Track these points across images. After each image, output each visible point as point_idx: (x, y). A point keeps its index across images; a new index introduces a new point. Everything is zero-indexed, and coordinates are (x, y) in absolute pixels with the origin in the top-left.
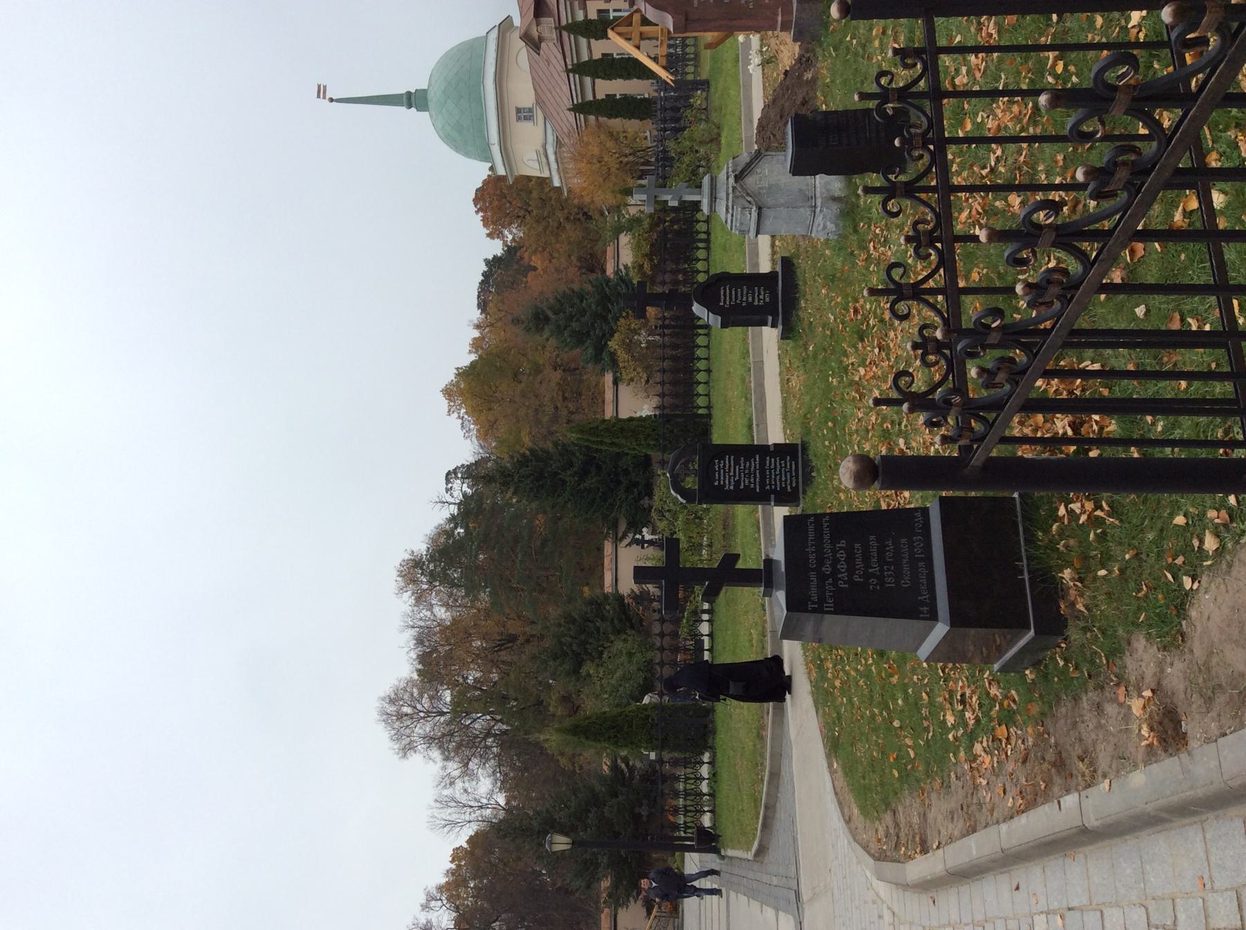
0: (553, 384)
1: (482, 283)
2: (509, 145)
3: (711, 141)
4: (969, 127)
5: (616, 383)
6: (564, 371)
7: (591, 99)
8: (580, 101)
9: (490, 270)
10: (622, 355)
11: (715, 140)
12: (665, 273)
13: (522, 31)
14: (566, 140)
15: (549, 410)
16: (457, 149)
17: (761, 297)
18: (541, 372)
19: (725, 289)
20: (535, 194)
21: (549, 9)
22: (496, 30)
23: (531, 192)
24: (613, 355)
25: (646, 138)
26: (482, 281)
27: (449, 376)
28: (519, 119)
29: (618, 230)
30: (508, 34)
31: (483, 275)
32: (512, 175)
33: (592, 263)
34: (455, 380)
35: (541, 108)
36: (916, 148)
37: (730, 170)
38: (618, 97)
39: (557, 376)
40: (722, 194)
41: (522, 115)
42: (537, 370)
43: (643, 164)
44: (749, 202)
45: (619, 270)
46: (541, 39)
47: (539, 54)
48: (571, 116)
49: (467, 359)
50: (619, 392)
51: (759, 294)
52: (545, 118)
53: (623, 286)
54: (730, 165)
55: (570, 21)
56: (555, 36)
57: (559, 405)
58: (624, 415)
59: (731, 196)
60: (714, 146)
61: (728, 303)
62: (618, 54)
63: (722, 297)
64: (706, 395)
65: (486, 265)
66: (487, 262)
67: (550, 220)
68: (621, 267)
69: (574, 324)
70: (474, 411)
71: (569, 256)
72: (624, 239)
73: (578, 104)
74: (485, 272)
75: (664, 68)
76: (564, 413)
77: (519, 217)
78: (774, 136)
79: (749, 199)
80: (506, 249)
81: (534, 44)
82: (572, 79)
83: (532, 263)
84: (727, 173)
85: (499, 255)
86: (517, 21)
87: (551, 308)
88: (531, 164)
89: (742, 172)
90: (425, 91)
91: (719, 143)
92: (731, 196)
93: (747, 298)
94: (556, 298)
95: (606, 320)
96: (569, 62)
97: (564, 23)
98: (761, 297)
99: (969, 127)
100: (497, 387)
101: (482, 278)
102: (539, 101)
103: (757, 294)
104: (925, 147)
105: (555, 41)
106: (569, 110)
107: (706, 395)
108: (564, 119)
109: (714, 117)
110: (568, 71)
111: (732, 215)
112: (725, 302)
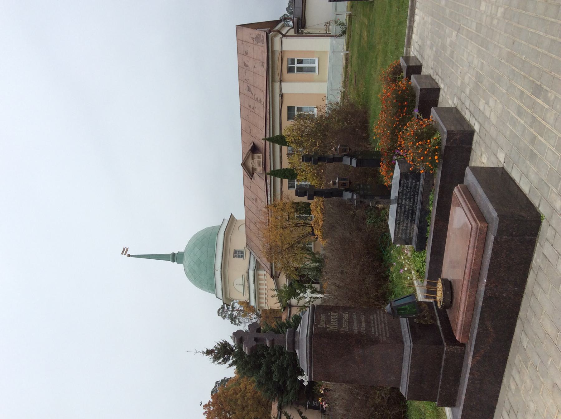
28: (235, 256)
41: (237, 255)
55: (271, 136)
82: (268, 181)
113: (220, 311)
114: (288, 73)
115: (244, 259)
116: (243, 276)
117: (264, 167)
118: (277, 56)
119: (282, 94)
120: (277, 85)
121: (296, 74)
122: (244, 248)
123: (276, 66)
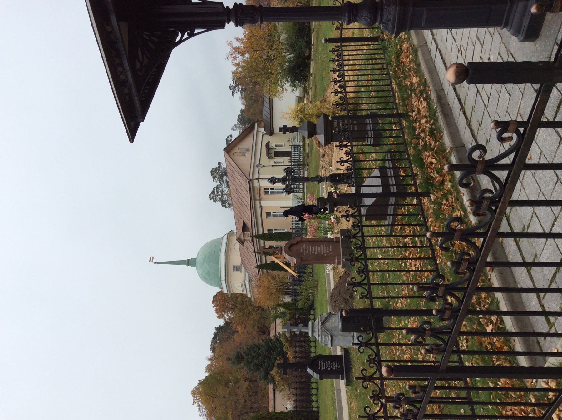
0: (244, 389)
1: (213, 338)
2: (229, 280)
3: (314, 287)
4: (403, 324)
5: (274, 390)
6: (250, 381)
7: (265, 263)
8: (260, 264)
9: (217, 332)
10: (277, 378)
11: (316, 286)
12: (296, 342)
13: (237, 237)
14: (254, 279)
15: (242, 401)
16: (207, 283)
17: (336, 366)
18: (238, 382)
19: (321, 362)
20: (239, 299)
21: (248, 229)
22: (226, 236)
23: (238, 298)
24: (273, 378)
25: (288, 278)
26: (214, 337)
27: (195, 384)
28: (234, 270)
29: (276, 317)
30: (231, 237)
31: (214, 334)
32: (230, 293)
33: (264, 330)
34: (197, 386)
35: (244, 266)
36: (372, 364)
37: (319, 320)
39: (246, 384)
40: (317, 330)
41: (236, 268)
42: (237, 381)
43: (287, 289)
44: (327, 333)
45: (276, 335)
46: (245, 240)
48: (256, 270)
49: (203, 375)
50: (276, 394)
51: (335, 365)
53: (278, 343)
54: (319, 318)
55: (257, 234)
57: (247, 400)
58: (278, 410)
59: (320, 331)
60: (315, 289)
61: (322, 368)
62: (276, 246)
63: (320, 366)
64: (316, 401)
65: (216, 330)
66: (216, 328)
67: (245, 310)
68: (277, 334)
69: (255, 361)
70: (205, 402)
71: (254, 326)
72: (278, 321)
73: (259, 265)
74: (215, 333)
75: (293, 271)
76: (249, 404)
77: (232, 309)
78: (337, 301)
79: (327, 332)
80: (225, 322)
81: (241, 242)
83: (237, 330)
84: (318, 321)
85: (222, 325)
86: (235, 231)
87: (244, 353)
88: (238, 288)
89: (324, 321)
90: (195, 259)
91: (317, 288)
92: (320, 331)
93: (330, 366)
94: (247, 348)
95: (270, 359)
96: (256, 249)
97: (254, 234)
98: (336, 366)
99: (403, 324)
100: (217, 390)
101: (214, 336)
102: (243, 263)
103: (334, 365)
104: (374, 363)
106: (256, 267)
107: (316, 401)
108: (253, 270)
109: (315, 278)
110: (255, 252)
111: (321, 338)
112: (321, 368)
115: (151, 261)
120: (258, 202)
121: (269, 196)
123: (256, 192)
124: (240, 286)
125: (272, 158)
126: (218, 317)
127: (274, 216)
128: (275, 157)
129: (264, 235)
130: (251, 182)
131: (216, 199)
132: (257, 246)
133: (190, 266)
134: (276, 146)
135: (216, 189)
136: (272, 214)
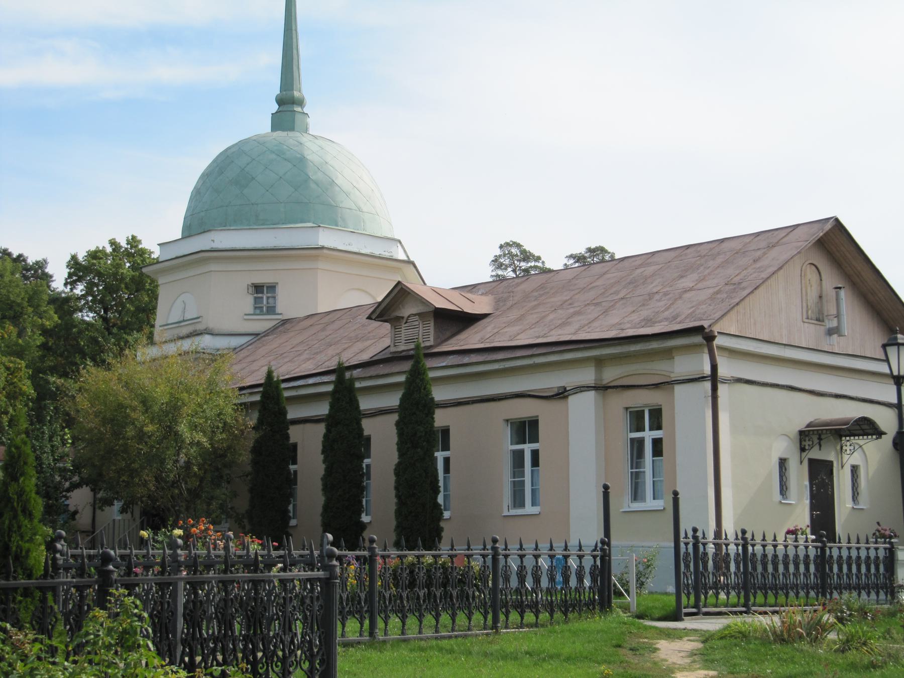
2: (213, 267)
7: (290, 416)
9: (27, 268)
16: (207, 176)
31: (20, 256)
38: (292, 467)
47: (369, 318)
48: (259, 377)
52: (257, 335)
56: (402, 348)
65: (37, 263)
82: (326, 379)
96: (356, 373)
105: (393, 349)
106: (269, 374)
110: (340, 370)
113: (514, 251)
114: (627, 409)
115: (246, 317)
116: (198, 318)
117: (404, 353)
118: (660, 369)
119: (566, 397)
120: (587, 376)
121: (624, 435)
122: (281, 314)
124: (188, 316)
125: (803, 449)
126: (74, 258)
127: (518, 457)
128: (806, 463)
129: (429, 407)
130: (698, 339)
131: (502, 264)
132: (371, 378)
133: (275, 107)
134: (855, 469)
135: (540, 264)
136: (527, 448)
